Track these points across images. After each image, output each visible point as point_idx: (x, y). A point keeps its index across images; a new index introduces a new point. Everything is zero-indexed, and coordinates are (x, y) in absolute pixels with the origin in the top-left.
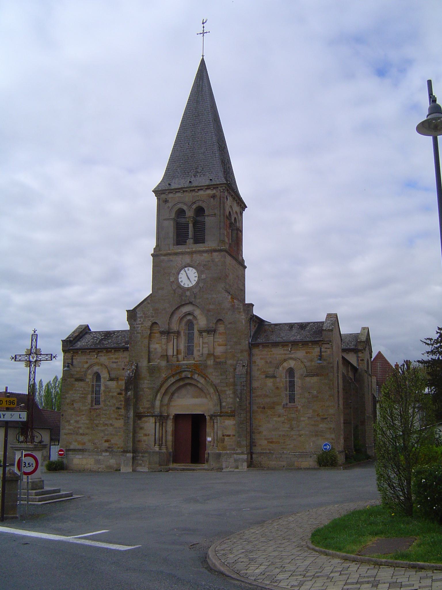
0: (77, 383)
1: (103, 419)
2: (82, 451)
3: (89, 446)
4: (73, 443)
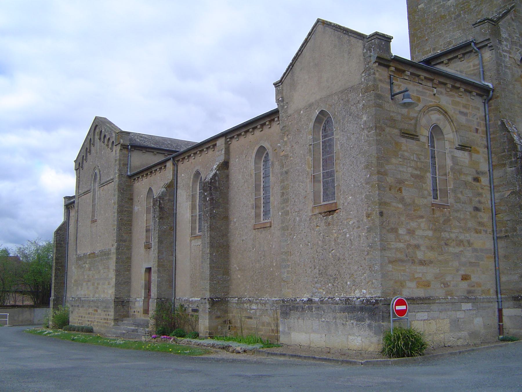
0: (403, 140)
3: (438, 291)
4: (409, 284)
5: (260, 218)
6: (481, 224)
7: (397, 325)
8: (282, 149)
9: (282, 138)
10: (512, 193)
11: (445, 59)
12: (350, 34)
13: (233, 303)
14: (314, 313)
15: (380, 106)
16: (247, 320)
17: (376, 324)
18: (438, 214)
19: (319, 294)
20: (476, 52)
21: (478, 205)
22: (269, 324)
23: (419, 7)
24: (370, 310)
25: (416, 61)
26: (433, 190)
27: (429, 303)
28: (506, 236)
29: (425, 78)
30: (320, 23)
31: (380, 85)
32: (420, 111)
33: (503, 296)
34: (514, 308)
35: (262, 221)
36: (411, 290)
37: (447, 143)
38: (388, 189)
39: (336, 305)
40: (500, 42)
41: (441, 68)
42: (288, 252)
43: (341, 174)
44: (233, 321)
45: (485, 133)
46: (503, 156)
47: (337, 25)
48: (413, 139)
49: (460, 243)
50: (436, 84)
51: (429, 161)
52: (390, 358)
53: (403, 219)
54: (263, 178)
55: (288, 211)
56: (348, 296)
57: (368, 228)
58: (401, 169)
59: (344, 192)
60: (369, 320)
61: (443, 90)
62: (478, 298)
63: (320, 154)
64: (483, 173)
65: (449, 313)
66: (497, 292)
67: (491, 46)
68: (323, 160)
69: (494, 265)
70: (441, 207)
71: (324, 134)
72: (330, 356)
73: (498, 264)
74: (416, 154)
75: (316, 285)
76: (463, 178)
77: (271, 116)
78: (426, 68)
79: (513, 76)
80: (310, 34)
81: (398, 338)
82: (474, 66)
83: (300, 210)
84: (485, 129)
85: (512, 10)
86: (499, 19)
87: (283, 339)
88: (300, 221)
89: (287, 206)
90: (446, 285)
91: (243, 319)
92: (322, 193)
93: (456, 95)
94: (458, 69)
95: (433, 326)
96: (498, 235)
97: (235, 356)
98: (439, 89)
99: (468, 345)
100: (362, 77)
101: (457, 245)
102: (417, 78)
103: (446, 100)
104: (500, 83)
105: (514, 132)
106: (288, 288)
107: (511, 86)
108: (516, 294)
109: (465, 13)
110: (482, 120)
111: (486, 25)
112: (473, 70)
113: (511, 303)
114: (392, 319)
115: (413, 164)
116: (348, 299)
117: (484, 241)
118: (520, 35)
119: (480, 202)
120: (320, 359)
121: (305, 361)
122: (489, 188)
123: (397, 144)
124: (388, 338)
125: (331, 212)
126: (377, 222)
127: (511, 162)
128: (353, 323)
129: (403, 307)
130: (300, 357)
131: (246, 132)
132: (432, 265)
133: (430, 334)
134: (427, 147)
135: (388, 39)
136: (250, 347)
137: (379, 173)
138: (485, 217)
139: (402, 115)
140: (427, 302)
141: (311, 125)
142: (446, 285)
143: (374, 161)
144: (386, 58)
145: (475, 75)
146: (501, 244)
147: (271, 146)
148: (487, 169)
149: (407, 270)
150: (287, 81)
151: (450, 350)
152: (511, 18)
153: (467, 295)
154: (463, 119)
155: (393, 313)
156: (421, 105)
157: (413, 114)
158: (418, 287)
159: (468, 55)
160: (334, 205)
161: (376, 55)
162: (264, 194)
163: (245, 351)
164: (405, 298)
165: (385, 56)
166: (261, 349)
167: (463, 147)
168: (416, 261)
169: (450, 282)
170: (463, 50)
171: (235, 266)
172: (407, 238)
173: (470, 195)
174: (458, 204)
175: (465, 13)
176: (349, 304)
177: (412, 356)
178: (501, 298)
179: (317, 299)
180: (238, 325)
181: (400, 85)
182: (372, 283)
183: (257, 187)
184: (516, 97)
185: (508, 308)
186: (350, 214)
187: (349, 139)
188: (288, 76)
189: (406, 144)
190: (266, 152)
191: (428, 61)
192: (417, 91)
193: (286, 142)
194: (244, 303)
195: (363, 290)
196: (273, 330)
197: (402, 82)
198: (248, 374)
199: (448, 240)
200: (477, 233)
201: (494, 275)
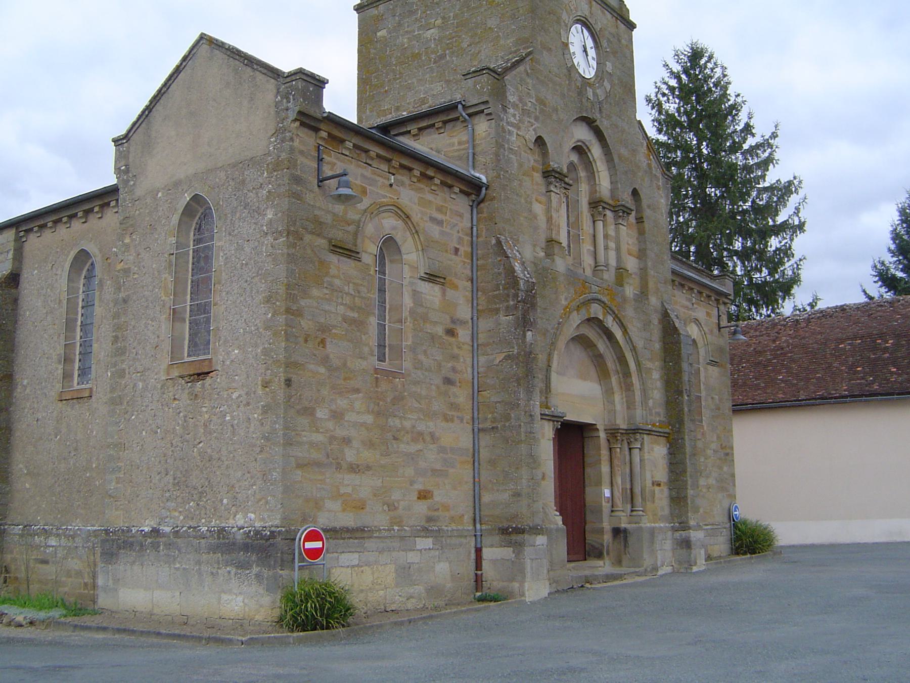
0: (334, 258)
1: (414, 416)
2: (355, 534)
3: (378, 518)
4: (329, 504)
5: (73, 381)
6: (454, 406)
7: (306, 575)
8: (120, 257)
9: (121, 238)
10: (508, 357)
11: (413, 128)
12: (255, 67)
13: (15, 534)
14: (162, 553)
15: (297, 196)
16: (40, 566)
17: (271, 573)
18: (384, 386)
19: (172, 520)
20: (465, 121)
21: (451, 375)
22: (79, 574)
23: (379, 34)
24: (261, 549)
25: (365, 125)
26: (379, 346)
27: (363, 538)
28: (493, 428)
29: (378, 156)
30: (204, 41)
31: (301, 160)
32: (365, 211)
33: (484, 527)
34: (501, 546)
35: (76, 387)
36: (332, 515)
37: (406, 268)
38: (301, 340)
39: (202, 541)
40: (504, 108)
41: (407, 142)
42: (120, 443)
43: (222, 308)
44: (13, 567)
45: (470, 256)
46: (495, 297)
47: (234, 48)
48: (349, 257)
49: (418, 436)
50: (394, 167)
51: (375, 295)
52: (292, 631)
53: (325, 392)
54: (83, 307)
55: (124, 370)
56: (223, 525)
57: (263, 407)
58: (327, 307)
59: (226, 341)
60: (258, 565)
61: (406, 179)
62: (443, 530)
63: (187, 270)
64: (463, 323)
65: (394, 554)
66: (475, 520)
67: (490, 114)
68: (192, 282)
69: (472, 475)
70: (391, 375)
71: (197, 237)
72: (187, 631)
73: (479, 474)
74: (354, 283)
75: (169, 504)
76: (429, 328)
77: (103, 199)
78: (381, 139)
79: (521, 165)
80: (185, 59)
81: (308, 596)
82: (460, 143)
83: (146, 370)
84: (470, 249)
85: (527, 59)
86: (507, 70)
87: (103, 601)
88: (145, 389)
89: (123, 361)
90: (392, 507)
91: (32, 564)
92: (187, 342)
93: (427, 189)
94: (433, 146)
95: (367, 577)
96: (481, 426)
97: (13, 632)
98: (399, 177)
99: (425, 608)
100: (271, 142)
101: (413, 440)
102: (363, 155)
103: (409, 195)
104: (499, 176)
105: (515, 259)
106: (117, 510)
107: (516, 183)
108: (505, 525)
109: (453, 53)
110: (467, 235)
111: (485, 78)
112: (459, 150)
113: (497, 538)
114: (297, 564)
115: (347, 300)
116: (223, 529)
117: (458, 436)
118: (536, 100)
119: (454, 370)
120: (169, 636)
121: (142, 639)
122: (470, 348)
123: (322, 263)
124: (289, 598)
125: (202, 375)
126: (281, 396)
127: (507, 307)
128: (229, 572)
129: (318, 544)
130: (133, 632)
131: (56, 222)
132: (370, 473)
133: (362, 591)
134: (372, 272)
135: (319, 83)
136: (42, 615)
137: (288, 311)
138: (461, 396)
139: (334, 214)
140: (358, 535)
141: (175, 219)
142: (392, 507)
143: (282, 290)
144: (315, 115)
145: (460, 158)
146: (485, 440)
147: (100, 251)
148: (468, 316)
149: (328, 480)
150: (136, 137)
151: (394, 618)
152: (526, 71)
153: (427, 525)
154: (435, 231)
155: (300, 554)
156: (366, 202)
157: (353, 215)
158: (344, 510)
159: (451, 124)
160: (207, 363)
161: (297, 109)
162: (81, 338)
163: (31, 623)
164: (322, 529)
165: (312, 111)
166: (63, 619)
167: (431, 278)
168: (345, 466)
169: (398, 501)
170: (445, 115)
171: (21, 466)
172: (330, 425)
173: (439, 358)
174: (419, 373)
175: (453, 53)
176: (224, 538)
177: (328, 628)
178: (481, 530)
179: (167, 529)
180: (22, 575)
181: (335, 164)
182: (267, 502)
183: (70, 325)
184: (523, 201)
185: (492, 546)
186: (234, 381)
187: (240, 248)
188: (143, 125)
189: (338, 265)
190: (90, 261)
191: (385, 129)
192: (363, 176)
193: (127, 246)
194: (36, 534)
195: (249, 515)
196: (86, 584)
197: (337, 158)
198: (36, 664)
199: (398, 431)
200: (447, 420)
201: (472, 493)
